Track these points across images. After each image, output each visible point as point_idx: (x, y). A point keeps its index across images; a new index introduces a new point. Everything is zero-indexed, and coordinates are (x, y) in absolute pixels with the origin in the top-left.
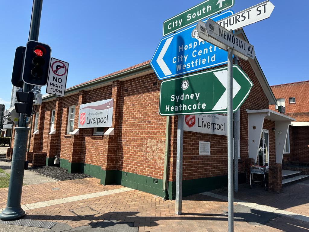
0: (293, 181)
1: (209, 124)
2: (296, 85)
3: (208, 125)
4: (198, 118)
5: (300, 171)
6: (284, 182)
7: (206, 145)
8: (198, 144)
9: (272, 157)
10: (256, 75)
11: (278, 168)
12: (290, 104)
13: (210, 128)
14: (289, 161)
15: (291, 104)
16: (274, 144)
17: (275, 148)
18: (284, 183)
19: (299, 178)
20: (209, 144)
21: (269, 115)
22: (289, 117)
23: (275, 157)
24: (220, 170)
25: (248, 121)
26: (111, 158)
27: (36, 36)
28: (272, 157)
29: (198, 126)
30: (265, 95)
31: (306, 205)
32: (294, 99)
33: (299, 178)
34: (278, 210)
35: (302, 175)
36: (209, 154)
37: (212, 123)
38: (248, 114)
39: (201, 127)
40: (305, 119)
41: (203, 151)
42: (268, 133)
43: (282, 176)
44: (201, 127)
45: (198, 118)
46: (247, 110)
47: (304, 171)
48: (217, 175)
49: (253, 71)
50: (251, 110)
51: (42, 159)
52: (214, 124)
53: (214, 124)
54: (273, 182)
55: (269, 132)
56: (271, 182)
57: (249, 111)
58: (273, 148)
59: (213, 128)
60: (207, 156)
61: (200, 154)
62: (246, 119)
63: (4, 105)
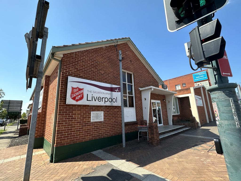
0: (175, 133)
1: (99, 98)
2: (185, 77)
3: (98, 99)
4: (87, 94)
5: (183, 125)
6: (161, 137)
7: (99, 114)
8: (90, 114)
9: (165, 118)
10: (147, 67)
11: (153, 127)
12: (183, 87)
13: (102, 101)
14: (179, 119)
15: (184, 87)
16: (166, 109)
17: (167, 112)
18: (165, 136)
19: (184, 129)
20: (102, 113)
21: (153, 90)
22: (173, 92)
23: (168, 117)
24: (114, 131)
25: (141, 96)
26: (38, 129)
27: (49, 64)
28: (165, 118)
29: (87, 100)
30: (155, 79)
31: (168, 159)
32: (185, 84)
33: (184, 129)
34: (140, 168)
35: (185, 127)
36: (103, 120)
37: (104, 98)
38: (141, 91)
39: (91, 101)
40: (186, 92)
41: (96, 118)
42: (160, 103)
43: (159, 133)
44: (91, 101)
45: (87, 94)
46: (139, 88)
47: (186, 125)
48: (112, 135)
49: (144, 65)
50: (142, 88)
51: (26, 131)
52: (105, 98)
53: (105, 98)
54: (151, 137)
55: (161, 102)
56: (150, 137)
57: (141, 89)
58: (166, 112)
59: (105, 101)
60: (101, 122)
61: (92, 121)
62: (140, 94)
63: (22, 101)
